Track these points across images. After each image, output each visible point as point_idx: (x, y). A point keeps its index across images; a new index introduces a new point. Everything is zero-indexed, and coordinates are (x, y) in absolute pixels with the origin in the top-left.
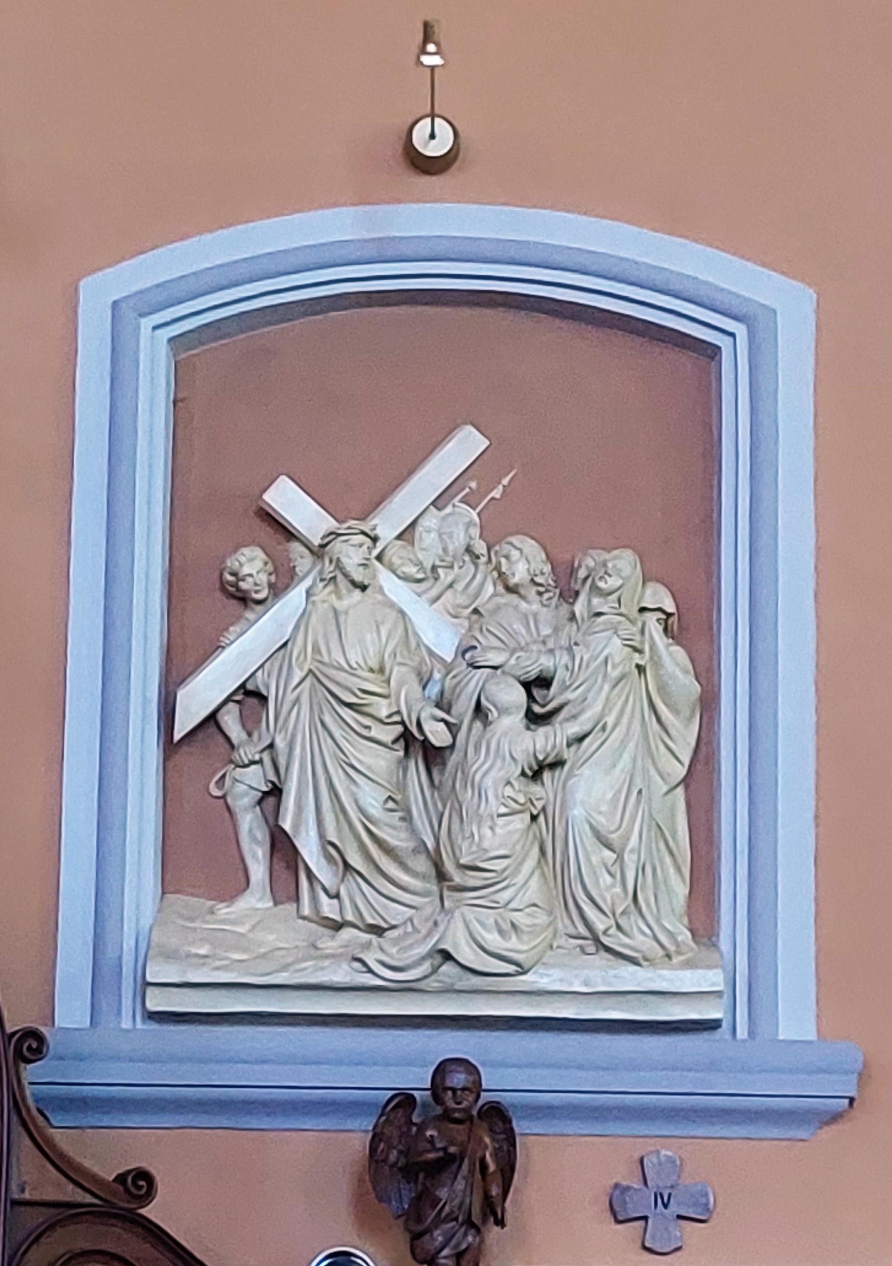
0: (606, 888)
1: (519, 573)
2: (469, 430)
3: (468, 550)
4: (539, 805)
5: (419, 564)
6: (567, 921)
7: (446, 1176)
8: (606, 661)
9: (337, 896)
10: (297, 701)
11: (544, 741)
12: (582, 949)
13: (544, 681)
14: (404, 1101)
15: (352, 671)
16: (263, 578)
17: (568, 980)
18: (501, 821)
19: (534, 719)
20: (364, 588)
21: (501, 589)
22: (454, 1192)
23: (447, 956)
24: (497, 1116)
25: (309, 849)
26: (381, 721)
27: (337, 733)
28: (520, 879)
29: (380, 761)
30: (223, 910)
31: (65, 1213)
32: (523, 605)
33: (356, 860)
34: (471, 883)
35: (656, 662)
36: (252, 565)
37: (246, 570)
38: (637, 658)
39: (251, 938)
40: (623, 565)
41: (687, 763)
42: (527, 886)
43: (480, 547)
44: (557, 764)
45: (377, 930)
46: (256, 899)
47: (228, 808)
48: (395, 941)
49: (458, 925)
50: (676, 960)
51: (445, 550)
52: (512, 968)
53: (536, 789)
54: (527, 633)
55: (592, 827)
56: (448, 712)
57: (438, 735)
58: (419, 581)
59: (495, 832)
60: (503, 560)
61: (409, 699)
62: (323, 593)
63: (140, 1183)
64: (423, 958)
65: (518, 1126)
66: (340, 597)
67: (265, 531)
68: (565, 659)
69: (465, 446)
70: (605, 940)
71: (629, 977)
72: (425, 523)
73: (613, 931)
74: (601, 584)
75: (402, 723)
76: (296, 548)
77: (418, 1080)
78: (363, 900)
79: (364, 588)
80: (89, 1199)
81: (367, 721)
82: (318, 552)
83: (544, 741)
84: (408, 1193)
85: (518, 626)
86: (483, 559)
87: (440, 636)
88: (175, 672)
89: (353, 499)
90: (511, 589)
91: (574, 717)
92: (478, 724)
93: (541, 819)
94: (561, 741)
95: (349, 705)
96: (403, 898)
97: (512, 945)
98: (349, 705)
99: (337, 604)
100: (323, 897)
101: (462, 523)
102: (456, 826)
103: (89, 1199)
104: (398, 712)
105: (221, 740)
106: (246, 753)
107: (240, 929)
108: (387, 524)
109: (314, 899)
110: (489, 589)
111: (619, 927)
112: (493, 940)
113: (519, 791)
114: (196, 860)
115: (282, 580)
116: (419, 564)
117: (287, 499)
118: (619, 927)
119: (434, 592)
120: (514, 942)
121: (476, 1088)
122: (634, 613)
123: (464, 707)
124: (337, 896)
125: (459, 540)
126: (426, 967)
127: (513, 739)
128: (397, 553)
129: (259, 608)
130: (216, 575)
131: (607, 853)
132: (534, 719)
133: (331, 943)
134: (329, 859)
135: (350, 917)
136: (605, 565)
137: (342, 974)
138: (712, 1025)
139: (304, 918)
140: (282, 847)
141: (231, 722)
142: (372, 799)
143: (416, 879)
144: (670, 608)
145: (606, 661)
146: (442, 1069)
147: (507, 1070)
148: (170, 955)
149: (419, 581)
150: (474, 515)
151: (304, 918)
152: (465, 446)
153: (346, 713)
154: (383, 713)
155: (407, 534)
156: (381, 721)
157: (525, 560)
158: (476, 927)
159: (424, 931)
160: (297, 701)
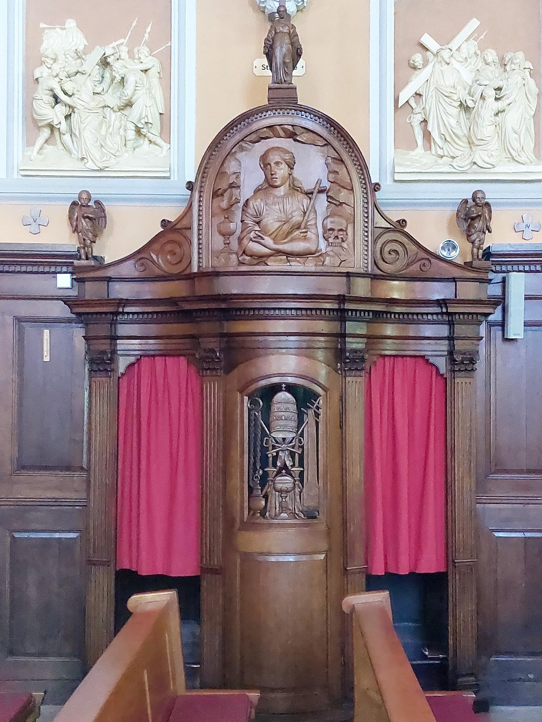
0: (516, 145)
1: (490, 59)
2: (475, 19)
3: (475, 53)
4: (498, 122)
5: (462, 57)
6: (504, 153)
7: (477, 220)
8: (517, 83)
9: (442, 149)
10: (432, 96)
11: (500, 105)
12: (509, 161)
13: (499, 89)
14: (466, 201)
15: (446, 87)
16: (421, 62)
17: (506, 170)
18: (488, 127)
19: (497, 99)
20: (448, 64)
21: (484, 64)
22: (479, 224)
23: (475, 163)
24: (487, 204)
25: (435, 135)
26: (454, 100)
27: (443, 104)
28: (494, 142)
29: (455, 111)
30: (412, 153)
31: (387, 230)
32: (490, 68)
33: (448, 139)
34: (481, 144)
35: (528, 83)
36: (418, 58)
37: (417, 60)
38: (524, 82)
39: (419, 161)
40: (520, 55)
41: (534, 110)
42: (494, 145)
43: (479, 52)
44: (504, 111)
45: (453, 158)
46: (420, 150)
47: (412, 126)
48: (460, 160)
49: (477, 156)
50: (533, 163)
51: (469, 53)
52: (491, 166)
53: (497, 118)
54: (493, 76)
55: (513, 128)
56: (473, 97)
57: (470, 104)
58: (462, 62)
59: (486, 129)
60: (486, 56)
61: (463, 95)
62: (438, 66)
63: (402, 223)
64: (468, 165)
65: (493, 208)
66: (442, 66)
67: (420, 49)
68: (506, 83)
69: (474, 24)
70: (515, 158)
71: (523, 168)
72: (463, 46)
73: (517, 156)
74: (515, 61)
75: (461, 101)
76: (428, 53)
77: (469, 196)
78: (449, 150)
79: (448, 64)
80: (392, 227)
81: (451, 101)
82: (436, 55)
83: (500, 105)
84: (466, 225)
85: (490, 74)
86: (480, 56)
87: (468, 77)
88: (398, 89)
89: (445, 39)
90: (487, 64)
91: (508, 98)
92: (481, 101)
93: (498, 126)
94: (505, 104)
95: (446, 96)
96: (460, 148)
97: (492, 161)
98: (446, 96)
99: (441, 68)
100: (438, 149)
101: (473, 46)
102: (476, 129)
103: (392, 227)
104: (459, 98)
105: (410, 108)
106: (417, 111)
107: (416, 158)
108: (454, 45)
109: (436, 150)
110: (481, 64)
111: (519, 155)
112: (487, 159)
113: (493, 118)
114: (404, 140)
115: (426, 62)
116: (462, 57)
117: (427, 40)
118: (519, 155)
119: (466, 65)
120: (492, 159)
121: (484, 198)
122: (522, 69)
123: (477, 96)
124: (442, 149)
125: (472, 51)
126: (469, 166)
127: (492, 105)
128: (456, 54)
129: (419, 70)
130: (407, 63)
131: (516, 135)
132: (497, 99)
133: (441, 161)
134: (441, 138)
135: (446, 154)
136: (515, 56)
137: (447, 169)
138: (169, 178)
139: (433, 155)
140: (427, 135)
141: (412, 103)
142: (453, 122)
143: (463, 143)
144: (532, 68)
145: (517, 83)
146: (475, 193)
147: (491, 194)
148: (401, 165)
149: (462, 62)
150: (476, 43)
151: (433, 155)
152: (474, 24)
153: (446, 98)
154: (455, 99)
155: (458, 49)
156: (454, 100)
157: (491, 55)
158: (482, 156)
159: (467, 157)
160: (432, 96)
